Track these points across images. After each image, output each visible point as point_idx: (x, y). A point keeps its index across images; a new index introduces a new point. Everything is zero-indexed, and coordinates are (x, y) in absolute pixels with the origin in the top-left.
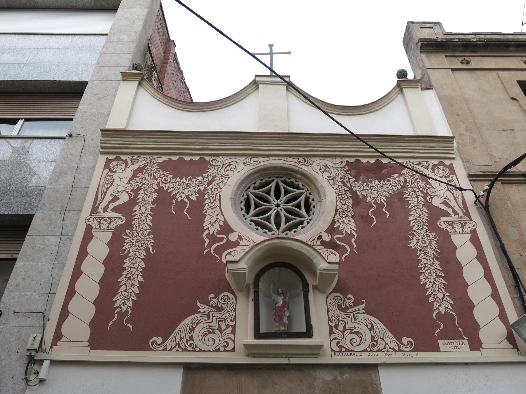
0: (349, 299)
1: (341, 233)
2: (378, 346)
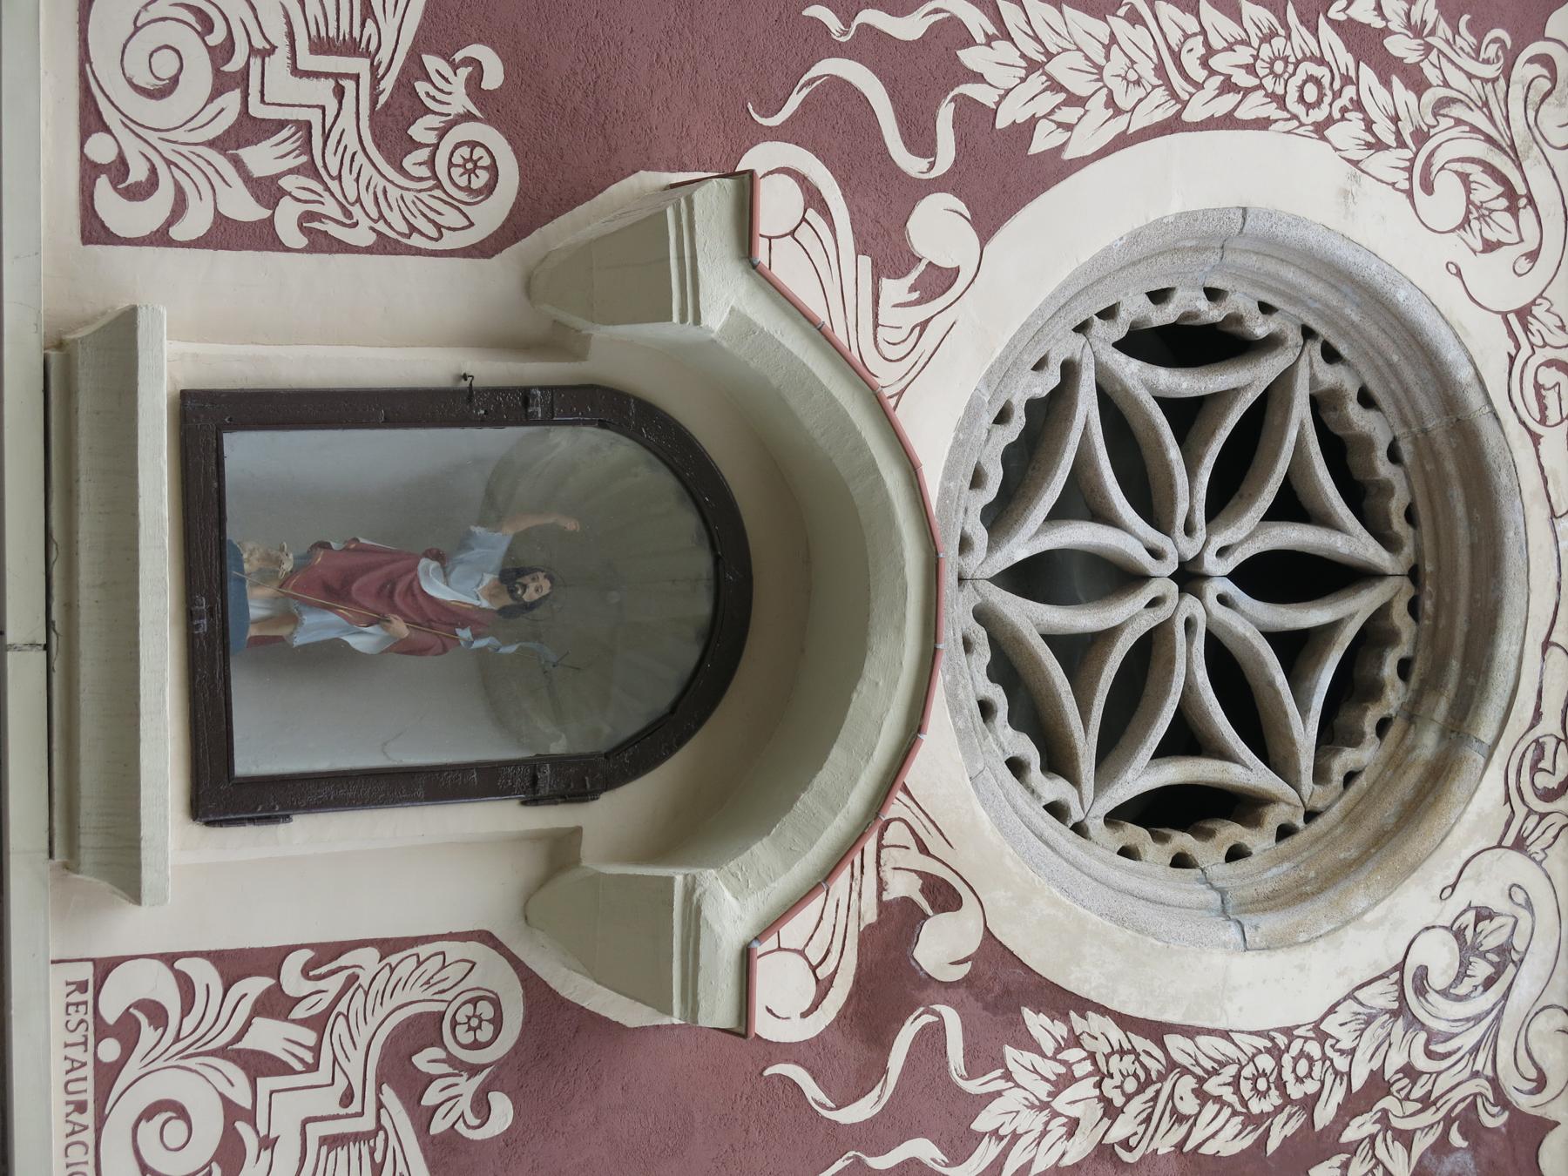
0: (482, 1107)
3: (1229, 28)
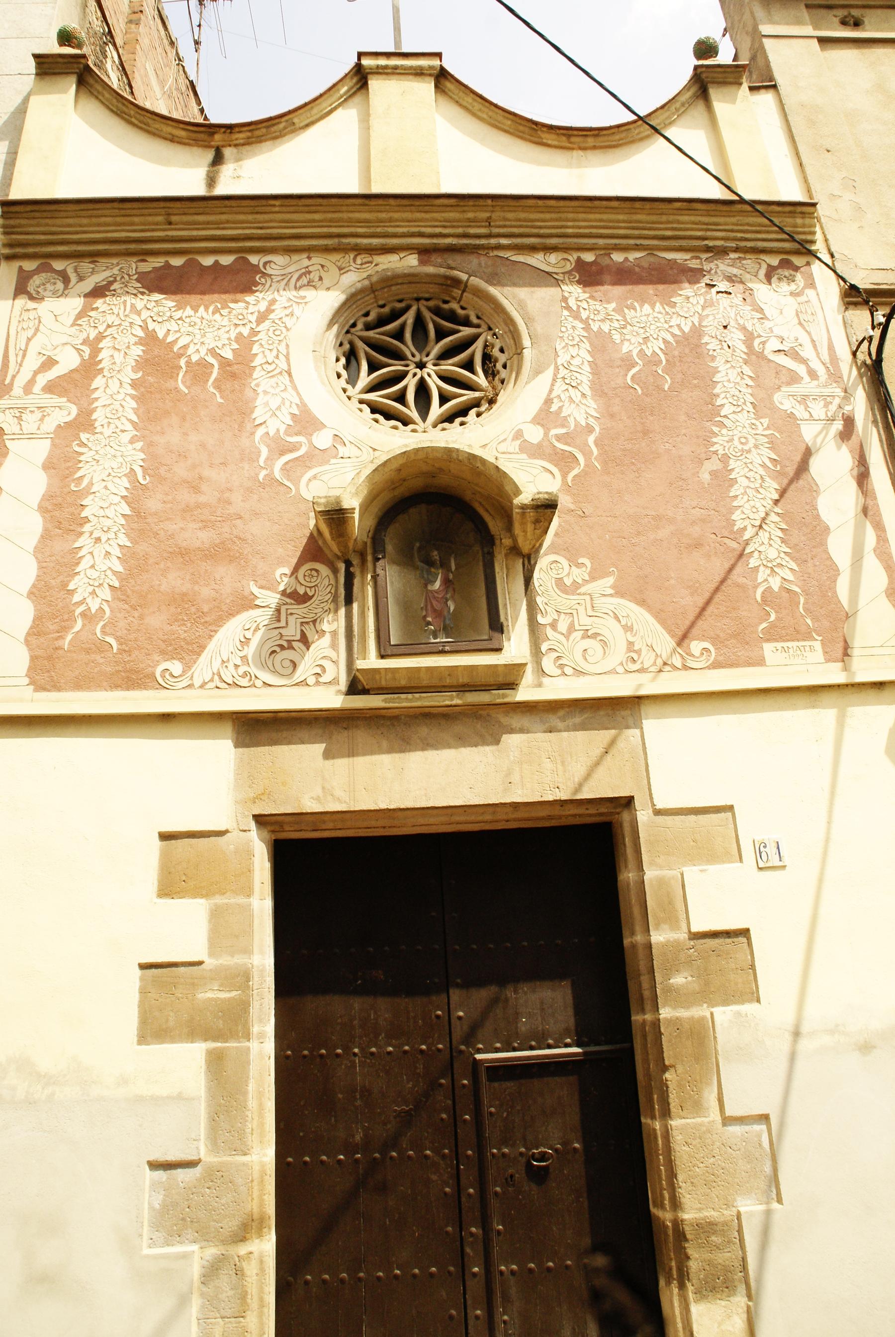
1: (564, 423)
2: (639, 662)
3: (260, 356)
